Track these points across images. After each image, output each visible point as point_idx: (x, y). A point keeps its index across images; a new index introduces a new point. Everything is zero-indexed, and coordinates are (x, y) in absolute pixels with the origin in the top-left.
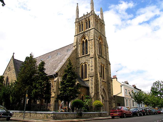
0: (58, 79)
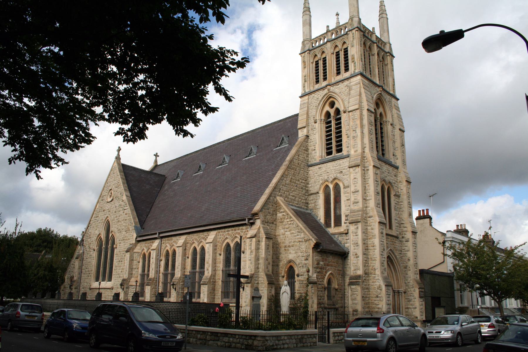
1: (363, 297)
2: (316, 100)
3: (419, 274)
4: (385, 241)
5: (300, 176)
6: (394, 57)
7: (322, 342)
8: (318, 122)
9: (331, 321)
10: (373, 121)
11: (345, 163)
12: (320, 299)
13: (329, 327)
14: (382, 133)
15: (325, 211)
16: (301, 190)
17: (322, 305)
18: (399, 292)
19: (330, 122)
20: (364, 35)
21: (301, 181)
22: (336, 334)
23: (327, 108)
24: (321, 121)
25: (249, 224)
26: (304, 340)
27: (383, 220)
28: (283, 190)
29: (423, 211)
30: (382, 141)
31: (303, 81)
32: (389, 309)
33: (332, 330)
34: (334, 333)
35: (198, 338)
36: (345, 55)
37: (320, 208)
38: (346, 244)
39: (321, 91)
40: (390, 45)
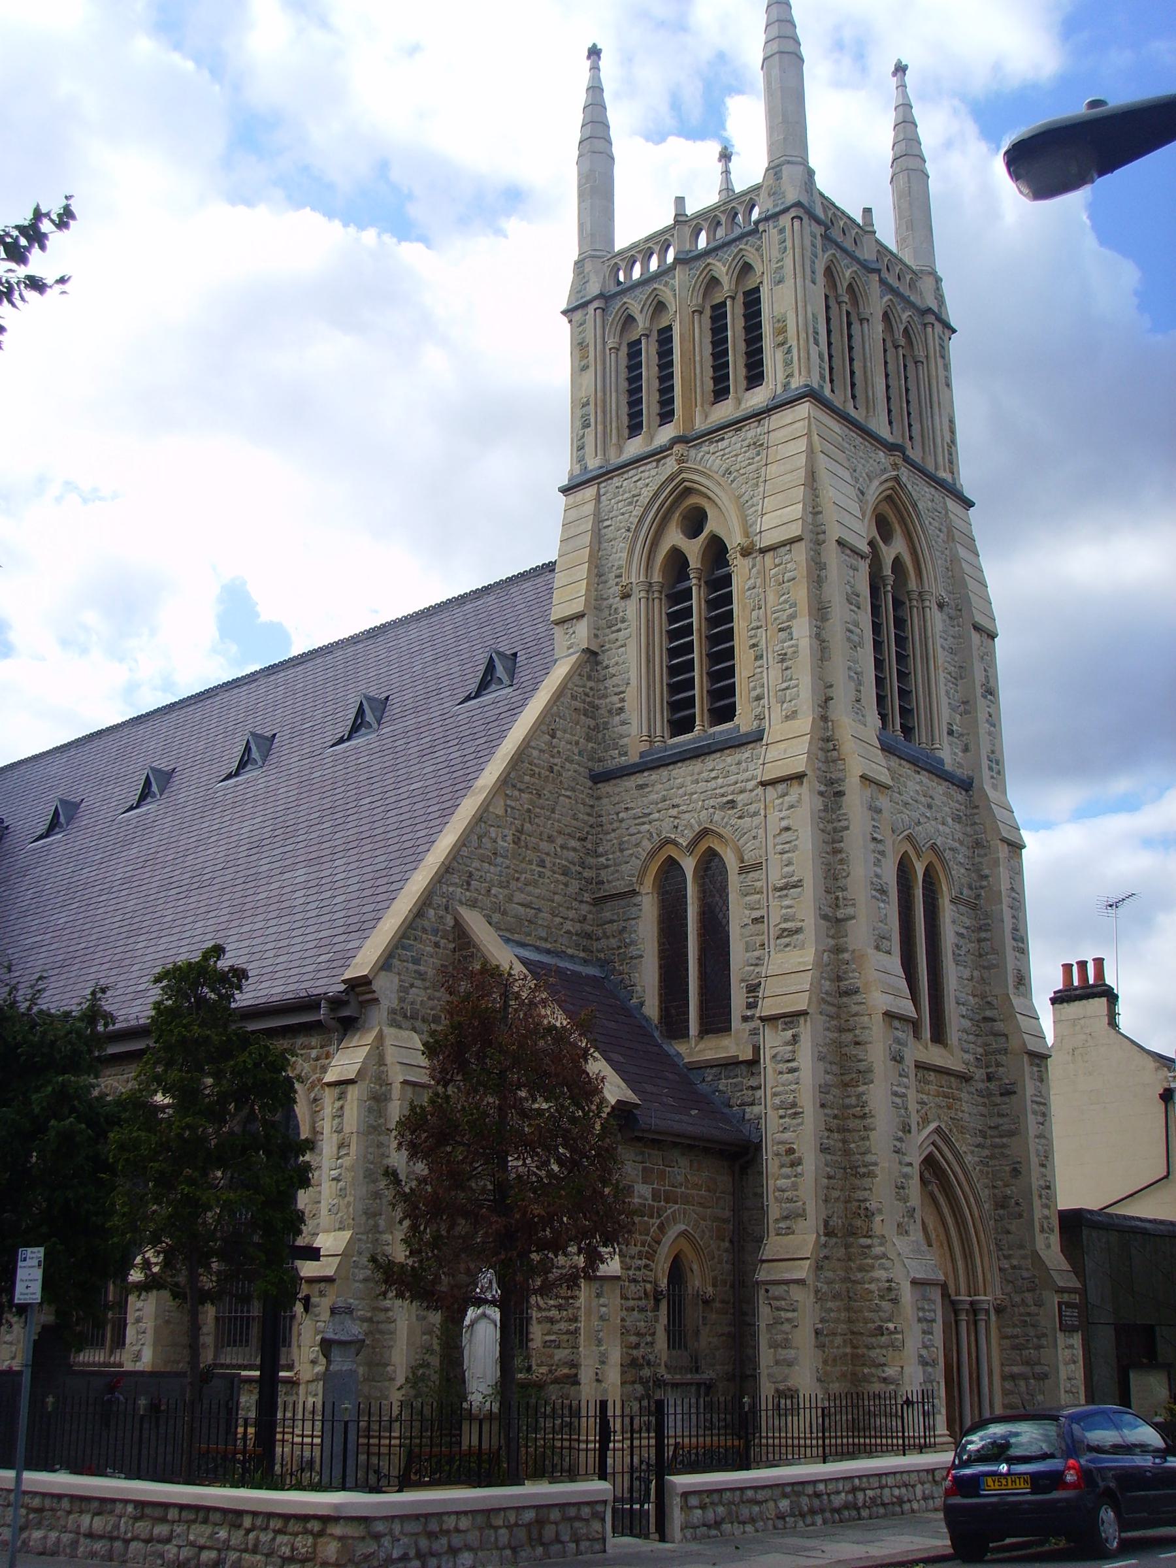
0: (378, 1055)
1: (817, 1333)
2: (630, 504)
3: (1057, 1229)
4: (912, 1095)
5: (559, 821)
6: (954, 331)
7: (632, 1535)
8: (638, 594)
9: (672, 1441)
10: (865, 591)
11: (744, 764)
12: (637, 1346)
13: (662, 1468)
14: (901, 641)
15: (660, 967)
16: (561, 878)
17: (646, 1372)
18: (974, 1309)
19: (687, 595)
20: (826, 237)
21: (560, 841)
22: (693, 1501)
23: (674, 537)
24: (648, 591)
25: (333, 1024)
26: (549, 1532)
27: (906, 1007)
28: (482, 879)
29: (1082, 965)
30: (903, 676)
31: (578, 424)
32: (931, 1382)
33: (683, 1481)
34: (685, 1495)
35: (82, 1530)
36: (747, 317)
37: (641, 956)
38: (748, 1109)
39: (649, 466)
40: (938, 280)
